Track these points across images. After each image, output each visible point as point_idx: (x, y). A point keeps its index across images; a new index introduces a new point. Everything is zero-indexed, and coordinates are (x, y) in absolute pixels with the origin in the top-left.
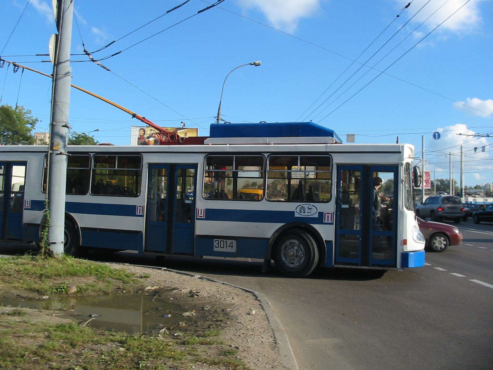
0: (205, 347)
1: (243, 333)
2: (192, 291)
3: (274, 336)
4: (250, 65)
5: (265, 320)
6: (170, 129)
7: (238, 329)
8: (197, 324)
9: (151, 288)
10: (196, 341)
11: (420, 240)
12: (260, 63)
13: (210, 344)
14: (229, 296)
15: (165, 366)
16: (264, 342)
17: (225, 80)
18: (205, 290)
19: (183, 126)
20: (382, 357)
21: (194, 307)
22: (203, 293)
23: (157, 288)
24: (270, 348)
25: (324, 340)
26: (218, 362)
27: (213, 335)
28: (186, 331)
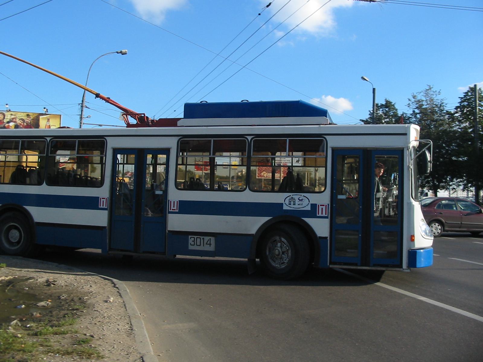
0: (59, 337)
1: (100, 321)
2: (48, 280)
3: (130, 323)
4: (116, 53)
5: (122, 307)
6: (32, 114)
7: (94, 317)
8: (52, 314)
9: (5, 278)
10: (49, 331)
11: (428, 236)
13: (64, 334)
14: (87, 284)
15: (13, 360)
16: (120, 329)
17: (90, 68)
18: (62, 279)
19: (46, 112)
20: (235, 339)
21: (50, 296)
22: (61, 282)
23: (12, 278)
24: (125, 335)
25: (180, 325)
26: (71, 351)
27: (67, 324)
28: (40, 321)
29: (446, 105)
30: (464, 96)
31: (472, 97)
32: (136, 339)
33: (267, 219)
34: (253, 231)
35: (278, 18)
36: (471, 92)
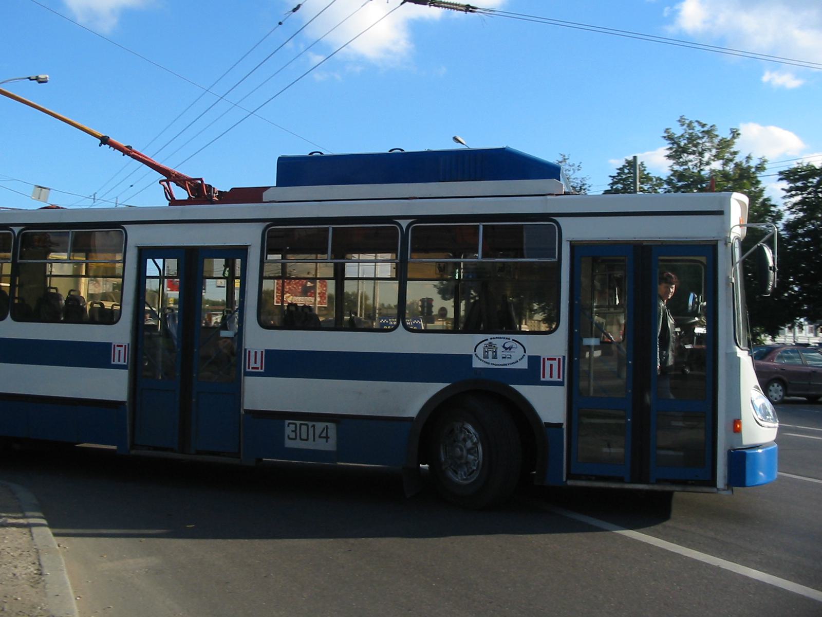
3: (39, 562)
4: (28, 80)
5: (25, 534)
12: (48, 79)
16: (18, 574)
20: (227, 583)
25: (131, 561)
29: (590, 189)
30: (618, 173)
31: (629, 177)
32: (47, 591)
33: (441, 386)
34: (413, 411)
35: (313, 32)
36: (628, 168)
